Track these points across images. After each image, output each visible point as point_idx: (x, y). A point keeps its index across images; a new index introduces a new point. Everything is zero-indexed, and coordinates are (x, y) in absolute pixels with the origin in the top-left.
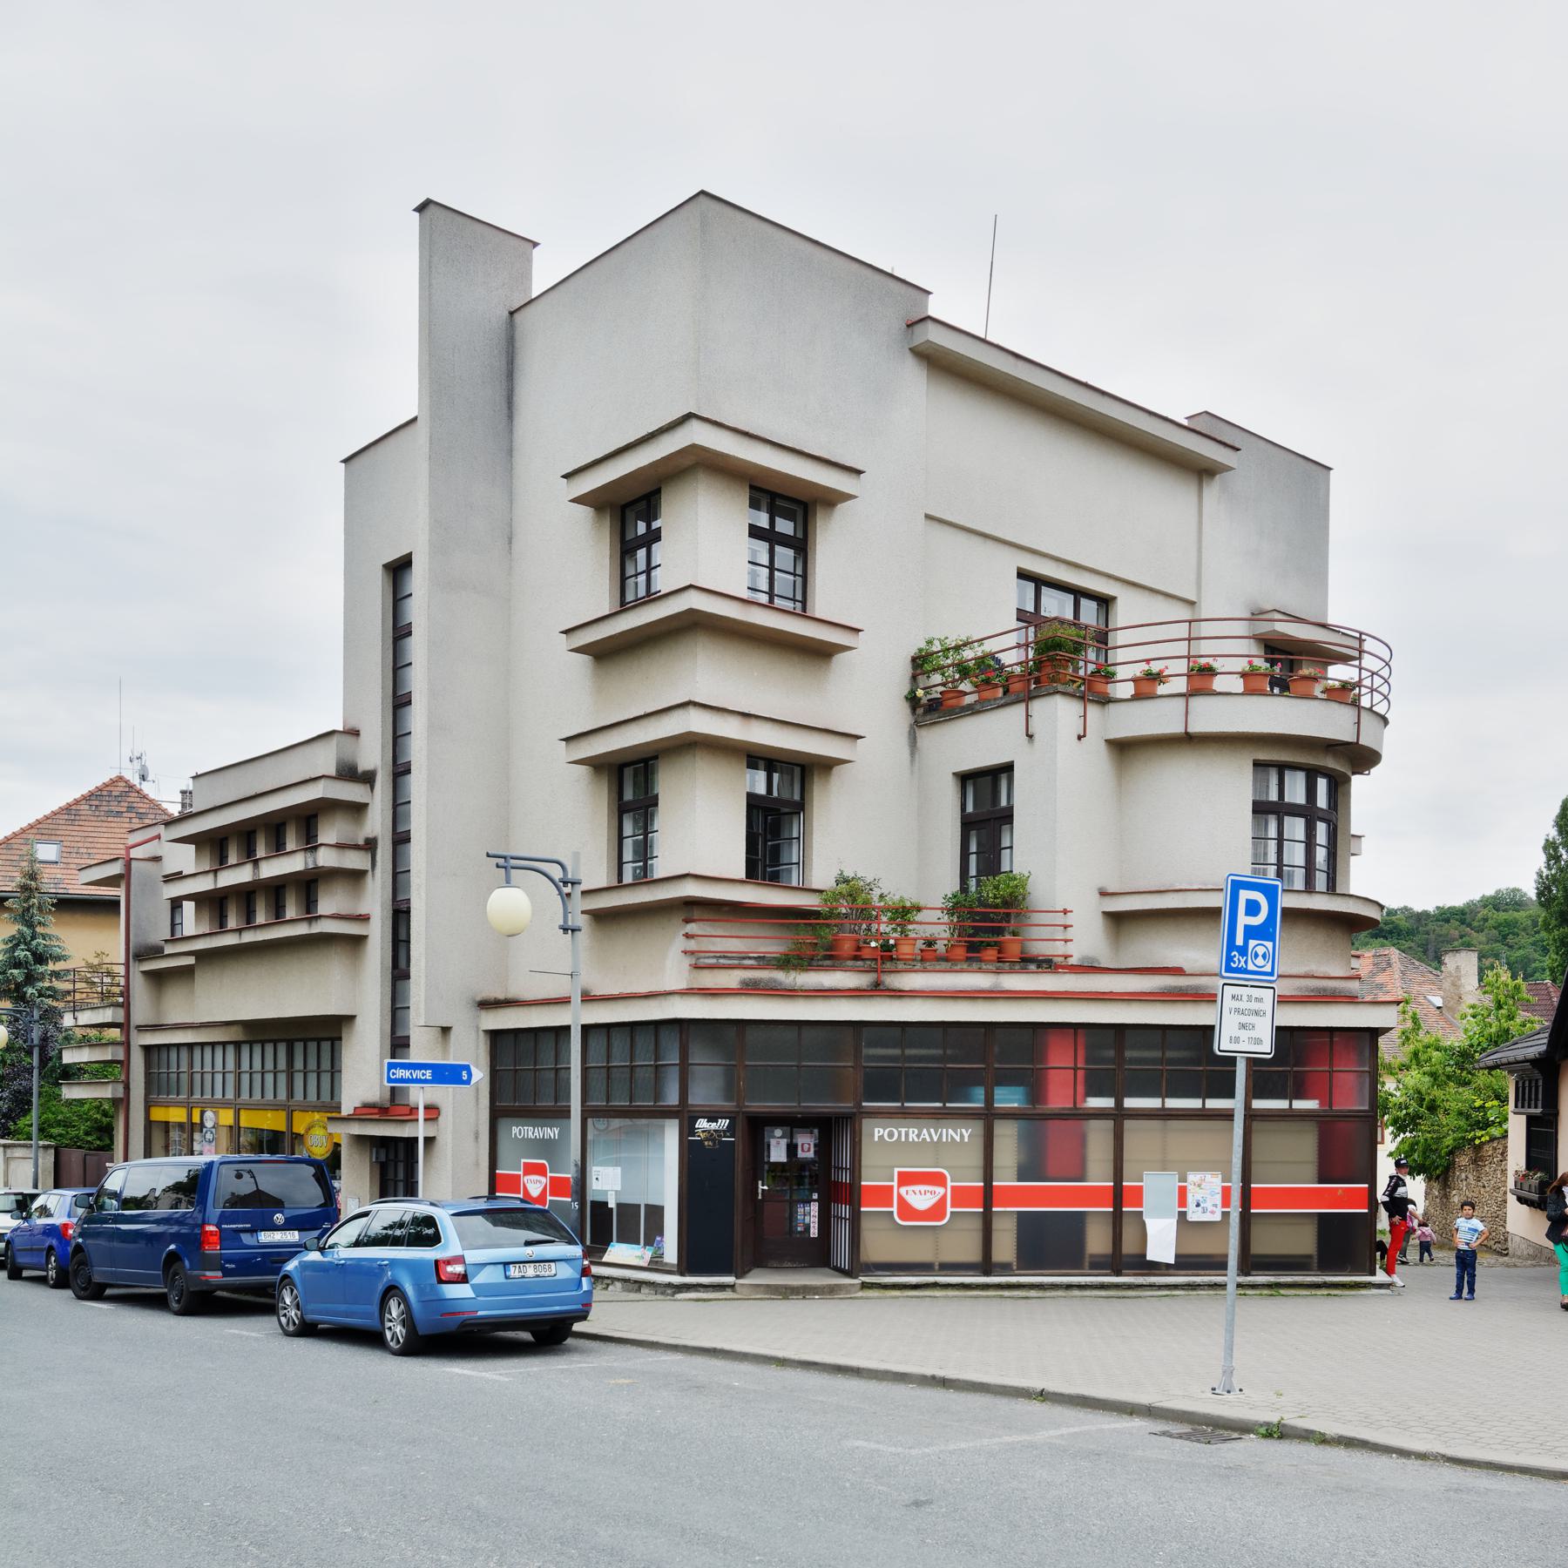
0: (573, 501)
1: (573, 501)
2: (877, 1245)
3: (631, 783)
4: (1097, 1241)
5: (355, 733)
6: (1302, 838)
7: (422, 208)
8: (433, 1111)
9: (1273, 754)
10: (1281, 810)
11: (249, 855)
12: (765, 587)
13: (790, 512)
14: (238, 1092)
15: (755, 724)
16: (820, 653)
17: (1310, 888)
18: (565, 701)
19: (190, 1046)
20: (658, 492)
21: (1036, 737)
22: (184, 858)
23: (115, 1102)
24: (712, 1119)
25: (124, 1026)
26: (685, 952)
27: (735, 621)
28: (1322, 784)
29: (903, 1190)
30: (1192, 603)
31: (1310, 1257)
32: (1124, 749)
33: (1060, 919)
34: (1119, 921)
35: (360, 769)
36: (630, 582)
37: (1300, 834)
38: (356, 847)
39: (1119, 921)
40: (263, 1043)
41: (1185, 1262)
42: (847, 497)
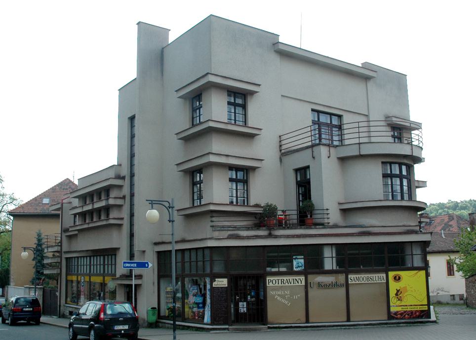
0: (179, 97)
1: (179, 97)
3: (194, 175)
5: (120, 165)
6: (399, 184)
7: (139, 24)
8: (139, 277)
9: (388, 159)
10: (392, 176)
11: (92, 202)
12: (234, 119)
13: (240, 97)
14: (78, 271)
15: (230, 158)
16: (251, 136)
17: (402, 198)
18: (176, 152)
19: (78, 257)
20: (201, 94)
21: (316, 157)
22: (76, 203)
23: (58, 274)
25: (60, 252)
26: (211, 226)
28: (404, 168)
30: (367, 115)
32: (343, 160)
34: (345, 212)
35: (121, 176)
36: (195, 119)
37: (398, 182)
38: (120, 198)
39: (345, 212)
40: (97, 256)
42: (257, 92)
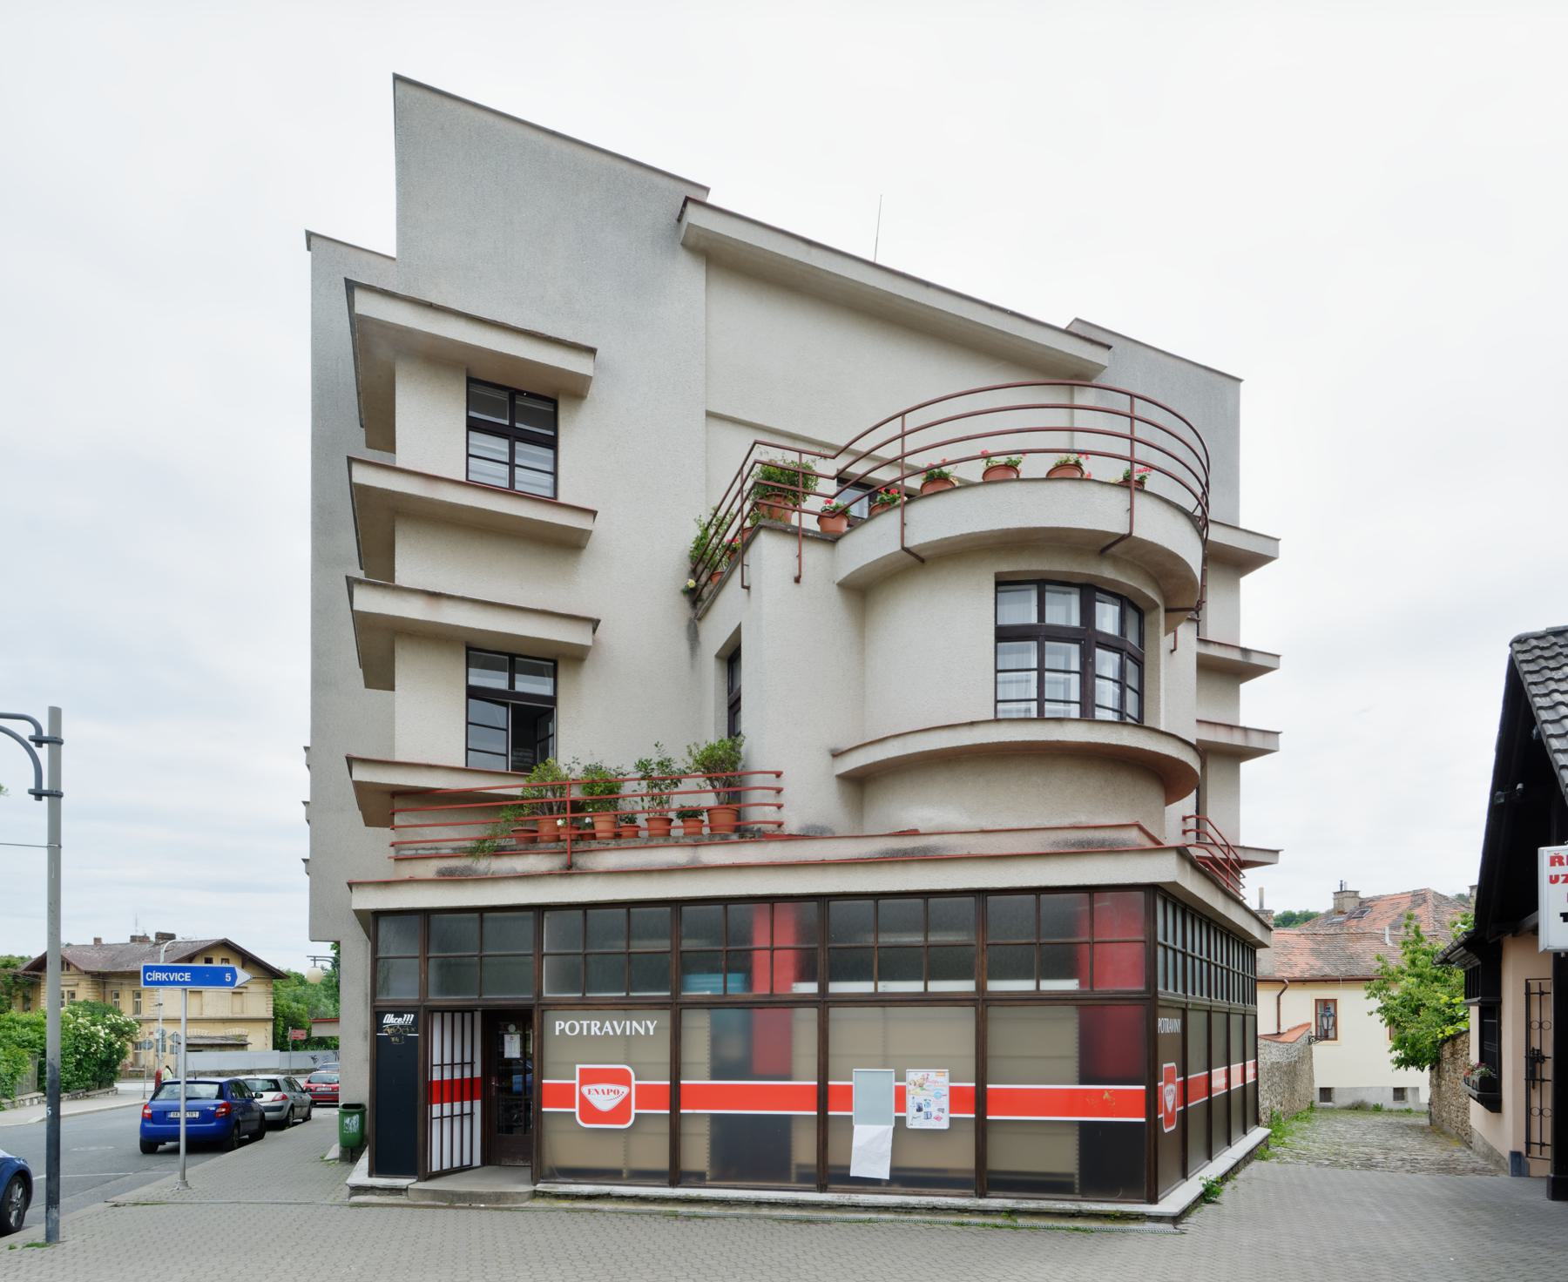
1: (739, 628)
2: (562, 1148)
4: (804, 1151)
10: (1040, 634)
13: (520, 405)
24: (398, 1014)
27: (420, 499)
29: (585, 1089)
31: (1072, 1175)
33: (771, 781)
39: (860, 784)
41: (902, 1178)
